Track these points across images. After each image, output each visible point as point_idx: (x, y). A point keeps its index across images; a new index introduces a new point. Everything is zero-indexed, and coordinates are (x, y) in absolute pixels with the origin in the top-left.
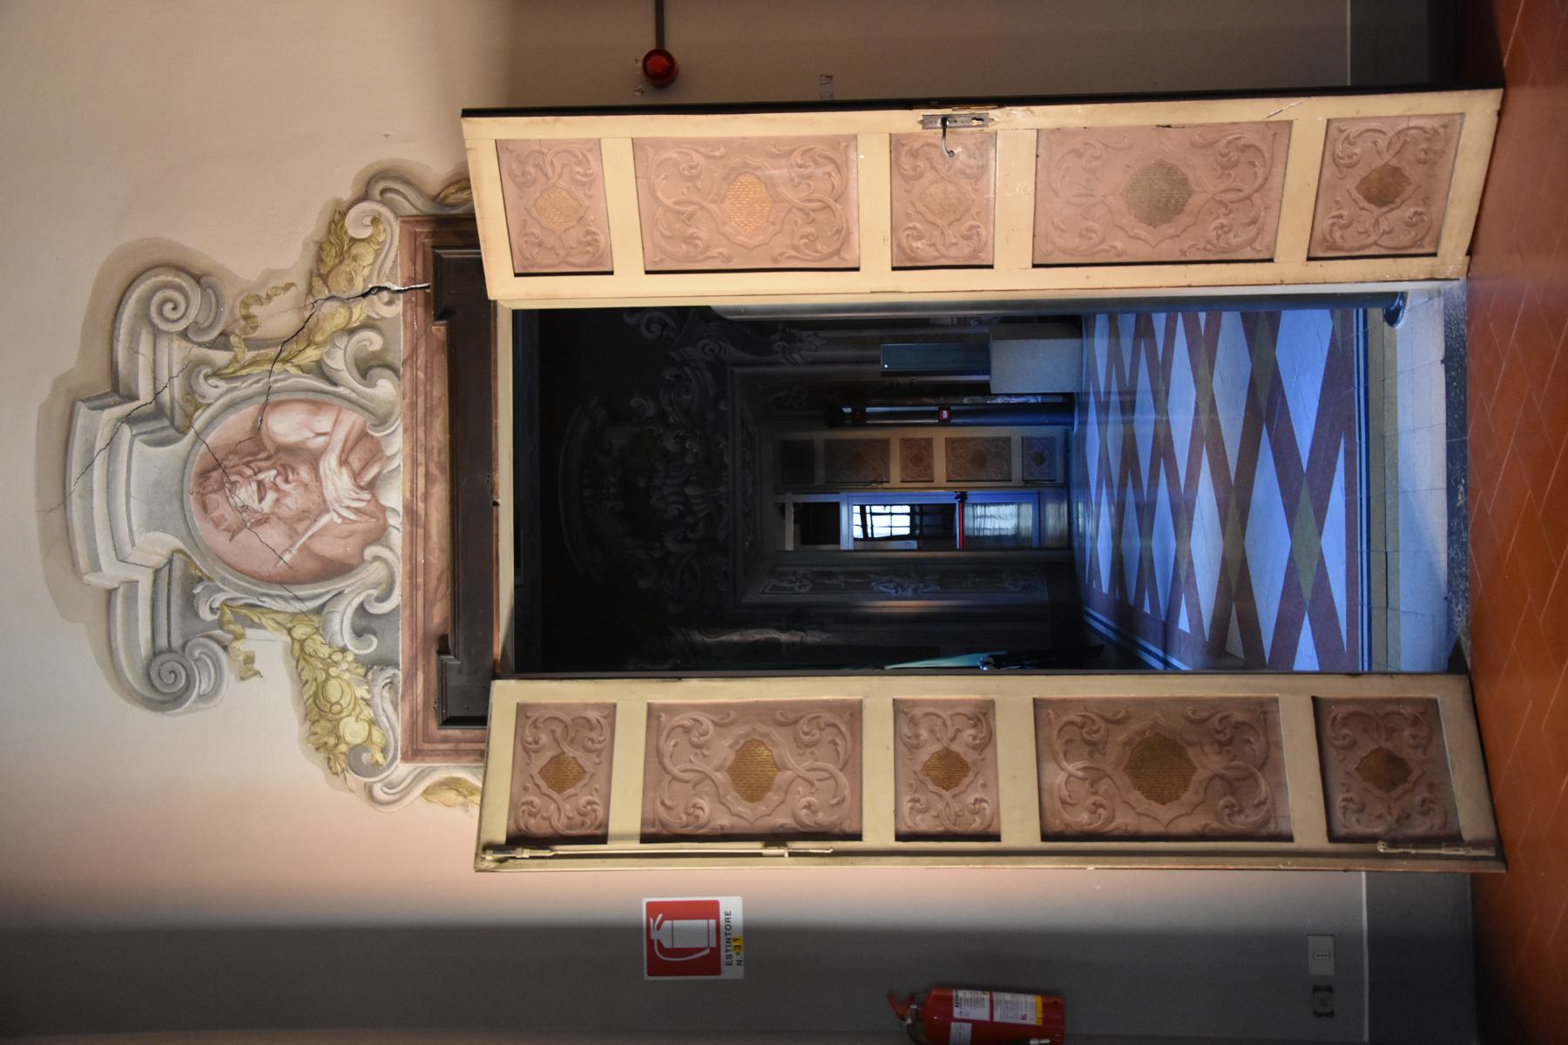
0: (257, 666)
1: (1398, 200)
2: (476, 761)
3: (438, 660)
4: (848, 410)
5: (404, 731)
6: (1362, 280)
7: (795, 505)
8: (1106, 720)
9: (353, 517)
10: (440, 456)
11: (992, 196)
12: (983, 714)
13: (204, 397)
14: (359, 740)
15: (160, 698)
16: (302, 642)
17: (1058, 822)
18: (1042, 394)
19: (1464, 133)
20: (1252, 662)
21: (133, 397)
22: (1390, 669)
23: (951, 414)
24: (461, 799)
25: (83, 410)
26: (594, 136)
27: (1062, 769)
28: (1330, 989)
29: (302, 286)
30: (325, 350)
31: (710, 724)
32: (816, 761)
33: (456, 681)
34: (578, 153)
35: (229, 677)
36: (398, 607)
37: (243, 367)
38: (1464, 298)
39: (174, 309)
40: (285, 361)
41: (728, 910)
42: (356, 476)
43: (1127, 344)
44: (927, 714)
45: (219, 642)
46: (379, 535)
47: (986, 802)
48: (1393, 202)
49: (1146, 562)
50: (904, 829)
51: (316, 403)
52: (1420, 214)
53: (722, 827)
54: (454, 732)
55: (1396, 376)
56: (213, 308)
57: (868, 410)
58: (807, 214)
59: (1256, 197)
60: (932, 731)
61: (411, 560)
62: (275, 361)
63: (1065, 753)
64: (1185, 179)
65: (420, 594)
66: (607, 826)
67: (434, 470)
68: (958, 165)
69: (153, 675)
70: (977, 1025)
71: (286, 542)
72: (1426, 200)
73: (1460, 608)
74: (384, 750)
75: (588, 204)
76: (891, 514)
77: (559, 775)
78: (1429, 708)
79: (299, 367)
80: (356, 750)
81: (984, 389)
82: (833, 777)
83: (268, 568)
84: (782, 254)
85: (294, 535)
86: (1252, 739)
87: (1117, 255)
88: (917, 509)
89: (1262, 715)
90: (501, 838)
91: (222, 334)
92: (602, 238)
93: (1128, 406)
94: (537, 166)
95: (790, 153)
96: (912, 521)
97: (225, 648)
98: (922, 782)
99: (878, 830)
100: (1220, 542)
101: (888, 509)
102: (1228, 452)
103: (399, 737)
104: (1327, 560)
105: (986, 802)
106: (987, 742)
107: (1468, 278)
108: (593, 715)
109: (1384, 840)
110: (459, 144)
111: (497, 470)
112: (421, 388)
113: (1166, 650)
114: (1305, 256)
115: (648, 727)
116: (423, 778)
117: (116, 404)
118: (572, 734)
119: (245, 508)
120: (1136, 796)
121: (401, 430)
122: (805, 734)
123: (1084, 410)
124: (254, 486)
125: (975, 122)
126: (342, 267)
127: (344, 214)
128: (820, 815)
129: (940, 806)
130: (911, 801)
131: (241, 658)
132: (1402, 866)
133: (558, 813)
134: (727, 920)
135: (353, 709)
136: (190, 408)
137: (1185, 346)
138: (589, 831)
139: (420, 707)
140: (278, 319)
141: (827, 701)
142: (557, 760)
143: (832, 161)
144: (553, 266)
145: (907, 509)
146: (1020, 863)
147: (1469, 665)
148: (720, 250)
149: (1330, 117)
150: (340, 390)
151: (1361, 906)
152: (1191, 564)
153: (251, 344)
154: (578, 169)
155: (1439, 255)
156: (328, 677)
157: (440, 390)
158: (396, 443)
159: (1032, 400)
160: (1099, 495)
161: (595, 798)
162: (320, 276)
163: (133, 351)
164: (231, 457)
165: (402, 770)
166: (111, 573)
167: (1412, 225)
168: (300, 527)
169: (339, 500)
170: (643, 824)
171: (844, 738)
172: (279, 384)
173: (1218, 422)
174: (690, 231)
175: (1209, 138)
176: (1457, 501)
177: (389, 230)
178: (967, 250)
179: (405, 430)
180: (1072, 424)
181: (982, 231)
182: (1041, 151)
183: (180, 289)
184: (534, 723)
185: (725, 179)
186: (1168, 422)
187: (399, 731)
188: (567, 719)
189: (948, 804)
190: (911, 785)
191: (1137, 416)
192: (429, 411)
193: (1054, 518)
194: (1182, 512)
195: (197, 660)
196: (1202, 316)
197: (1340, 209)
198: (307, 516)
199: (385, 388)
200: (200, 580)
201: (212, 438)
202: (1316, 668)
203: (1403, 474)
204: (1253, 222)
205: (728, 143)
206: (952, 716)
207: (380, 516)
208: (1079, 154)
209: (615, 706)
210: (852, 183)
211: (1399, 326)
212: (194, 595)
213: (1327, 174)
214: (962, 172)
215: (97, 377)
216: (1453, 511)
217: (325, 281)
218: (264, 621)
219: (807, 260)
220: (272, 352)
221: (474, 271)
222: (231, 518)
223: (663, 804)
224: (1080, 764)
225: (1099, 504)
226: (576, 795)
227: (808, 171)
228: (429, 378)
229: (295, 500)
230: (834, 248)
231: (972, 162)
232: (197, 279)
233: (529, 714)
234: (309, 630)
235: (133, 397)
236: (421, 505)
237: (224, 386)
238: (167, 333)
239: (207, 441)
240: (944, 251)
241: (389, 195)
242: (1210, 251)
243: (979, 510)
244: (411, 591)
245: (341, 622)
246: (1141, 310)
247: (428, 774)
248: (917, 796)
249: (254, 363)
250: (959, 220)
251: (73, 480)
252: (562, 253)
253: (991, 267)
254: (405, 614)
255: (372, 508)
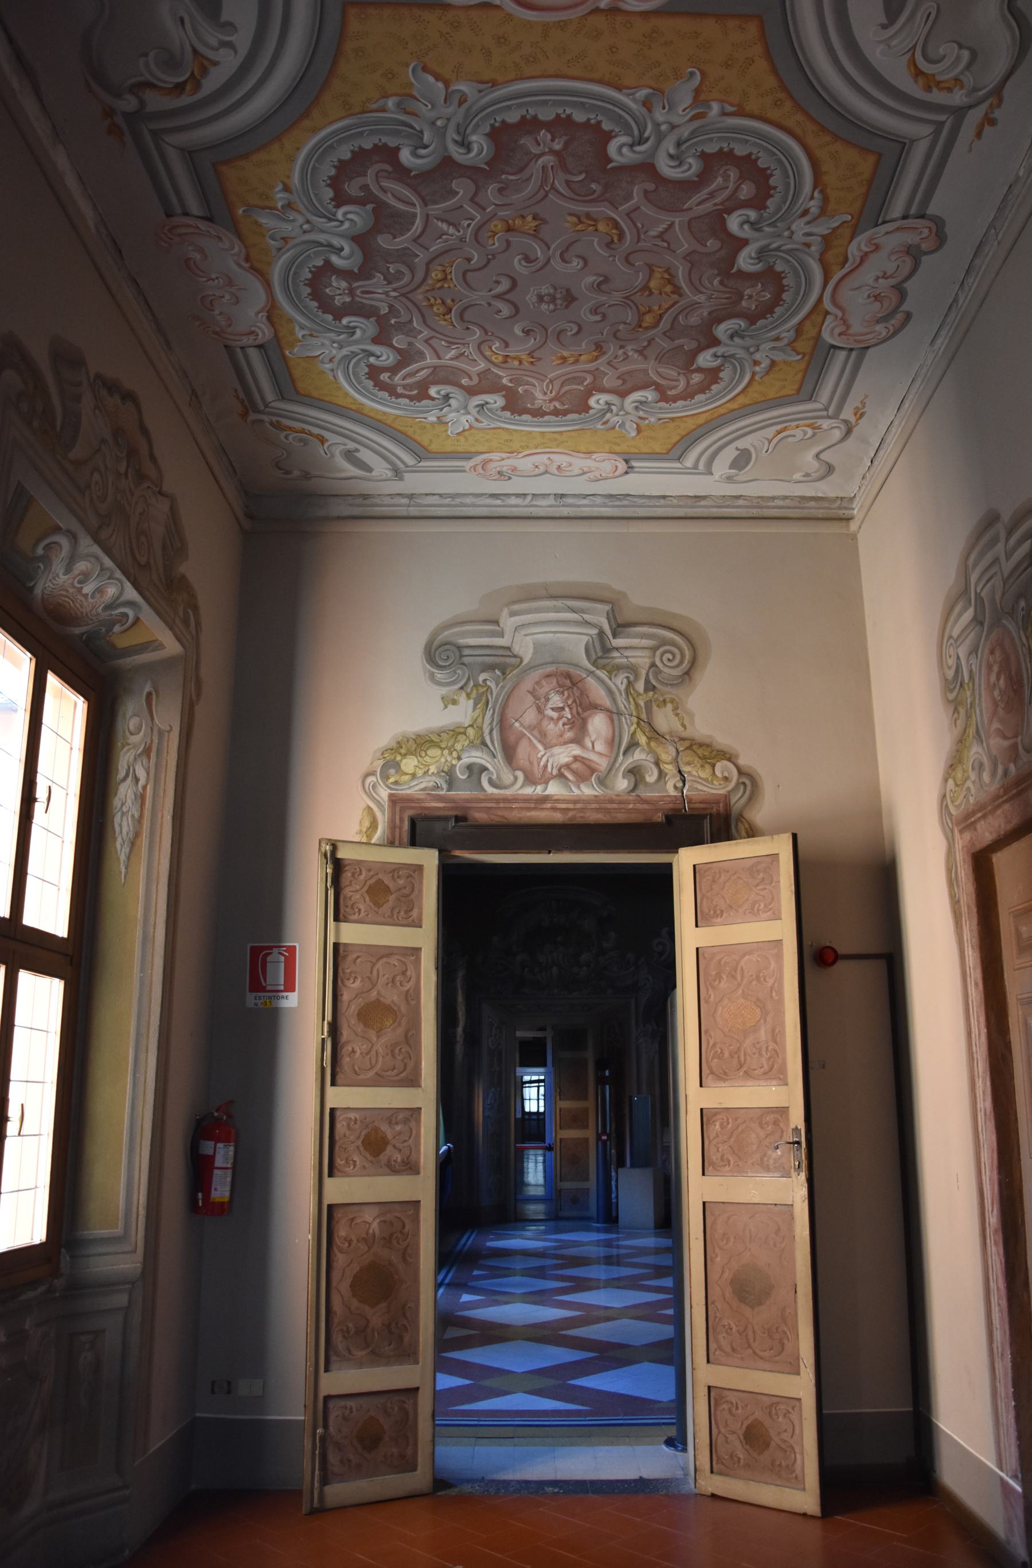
0: (450, 707)
1: (748, 1447)
2: (388, 839)
3: (451, 816)
4: (607, 1073)
5: (408, 795)
6: (696, 1422)
7: (545, 1038)
8: (406, 1249)
9: (542, 764)
10: (580, 818)
11: (750, 1175)
12: (410, 1167)
13: (615, 676)
14: (403, 767)
15: (433, 650)
16: (464, 733)
17: (340, 1215)
18: (617, 1203)
19: (793, 1491)
20: (442, 1345)
21: (615, 636)
22: (436, 1439)
23: (605, 1142)
24: (364, 830)
25: (607, 607)
26: (784, 915)
27: (374, 1219)
28: (229, 1392)
29: (684, 734)
30: (646, 747)
31: (408, 988)
32: (383, 1057)
33: (438, 826)
34: (772, 905)
35: (444, 691)
36: (485, 791)
37: (634, 699)
38: (683, 1492)
39: (669, 660)
40: (638, 724)
41: (289, 998)
42: (567, 766)
43: (651, 1260)
44: (411, 1130)
45: (466, 684)
46: (530, 780)
47: (354, 1167)
48: (746, 1443)
49: (507, 1272)
50: (338, 1113)
51: (613, 742)
52: (739, 1462)
53: (342, 995)
54: (406, 826)
55: (630, 1445)
56: (669, 682)
57: (607, 1087)
58: (736, 1053)
59: (750, 1351)
60: (400, 1133)
61: (514, 799)
62: (638, 718)
63: (385, 1222)
64: (761, 1304)
65: (494, 805)
66: (345, 922)
67: (571, 814)
68: (770, 1152)
69: (447, 647)
70: (211, 1159)
71: (527, 723)
72: (748, 1466)
73: (477, 1488)
74: (396, 783)
75: (740, 911)
76: (538, 1100)
77: (378, 891)
78: (409, 1465)
79: (634, 733)
80: (397, 766)
81: (621, 1163)
82: (372, 1068)
83: (510, 713)
84: (710, 1036)
85: (531, 728)
86: (391, 1346)
87: (711, 1258)
88: (541, 1117)
89: (408, 1354)
90: (340, 855)
91: (654, 687)
92: (719, 920)
93: (609, 1261)
94: (763, 879)
95: (776, 1042)
96: (534, 1113)
97: (462, 688)
98: (367, 1126)
99: (338, 1097)
100: (520, 1323)
101: (541, 1097)
102: (580, 1329)
103: (404, 792)
104: (508, 1397)
105: (354, 1167)
106: (393, 1169)
107: (696, 1495)
108: (415, 913)
109: (325, 1432)
110: (775, 831)
111: (571, 852)
112: (622, 806)
113: (449, 1285)
114: (711, 1385)
115: (407, 948)
116: (378, 807)
117: (611, 626)
118: (402, 899)
119: (548, 700)
120: (356, 1268)
121: (596, 793)
122: (400, 1050)
123: (607, 1231)
124: (561, 705)
125: (797, 1163)
126: (697, 759)
127: (729, 760)
128: (348, 1059)
129: (352, 1138)
130: (356, 1119)
131: (455, 697)
132: (308, 1445)
133: (354, 891)
134: (283, 997)
135: (422, 764)
136: (609, 668)
137: (649, 1300)
138: (342, 911)
139: (423, 805)
140: (664, 720)
141: (421, 1064)
142: (387, 890)
143: (771, 1070)
144: (701, 889)
145: (542, 1110)
146: (314, 1190)
147: (439, 1493)
148: (712, 996)
149: (803, 1401)
150: (621, 757)
151: (280, 1415)
152: (506, 1303)
153: (648, 704)
154: (762, 905)
155: (712, 1475)
156: (443, 749)
157: (621, 818)
158: (587, 791)
159: (613, 1196)
160: (551, 1240)
161: (363, 914)
162: (691, 745)
163: (643, 636)
164: (579, 692)
165: (384, 793)
166: (508, 623)
167: (731, 1456)
168: (536, 732)
169: (552, 756)
170: (345, 944)
171: (397, 1075)
172: (624, 720)
173: (599, 1323)
174: (725, 977)
175: (787, 1319)
176: (548, 1487)
177: (720, 787)
178: (714, 1158)
179: (596, 796)
180: (598, 1222)
181: (727, 1168)
182: (779, 1207)
183: (681, 662)
184: (410, 876)
185: (758, 999)
186: (598, 1288)
187: (409, 792)
188: (413, 896)
189: (353, 1143)
190: (365, 1119)
191: (603, 1267)
192: (608, 811)
193: (535, 1210)
194: (539, 1297)
195: (455, 672)
196: (670, 1312)
197: (742, 1408)
198: (543, 737)
199: (622, 784)
200: (504, 673)
201: (591, 681)
202: (438, 1388)
203: (564, 1445)
204: (733, 1350)
205: (781, 1001)
206: (409, 1146)
207: (542, 781)
208: (778, 1231)
209: (421, 927)
210: (757, 1083)
211: (664, 1447)
212: (494, 670)
213: (765, 1399)
214: (765, 1155)
215: (627, 615)
216: (541, 1484)
217: (687, 748)
218: (478, 711)
219: (706, 1052)
220: (644, 716)
221: (696, 840)
222: (542, 692)
223: (358, 957)
224: (377, 1231)
225: (545, 1240)
226: (365, 902)
227: (764, 1053)
228: (628, 811)
229: (552, 729)
230: (714, 1069)
231: (771, 1161)
232: (687, 673)
233: (417, 872)
234: (472, 738)
235: (615, 636)
236: (549, 806)
237: (623, 687)
238: (654, 656)
239: (589, 678)
240: (714, 1142)
241: (742, 787)
242: (715, 1320)
243: (540, 1159)
244: (495, 799)
245: (477, 757)
246: (676, 1269)
247: (380, 809)
248: (359, 1123)
249: (637, 705)
250: (734, 1152)
251: (565, 602)
252: (709, 895)
253: (703, 1174)
254: (481, 795)
255: (547, 776)
